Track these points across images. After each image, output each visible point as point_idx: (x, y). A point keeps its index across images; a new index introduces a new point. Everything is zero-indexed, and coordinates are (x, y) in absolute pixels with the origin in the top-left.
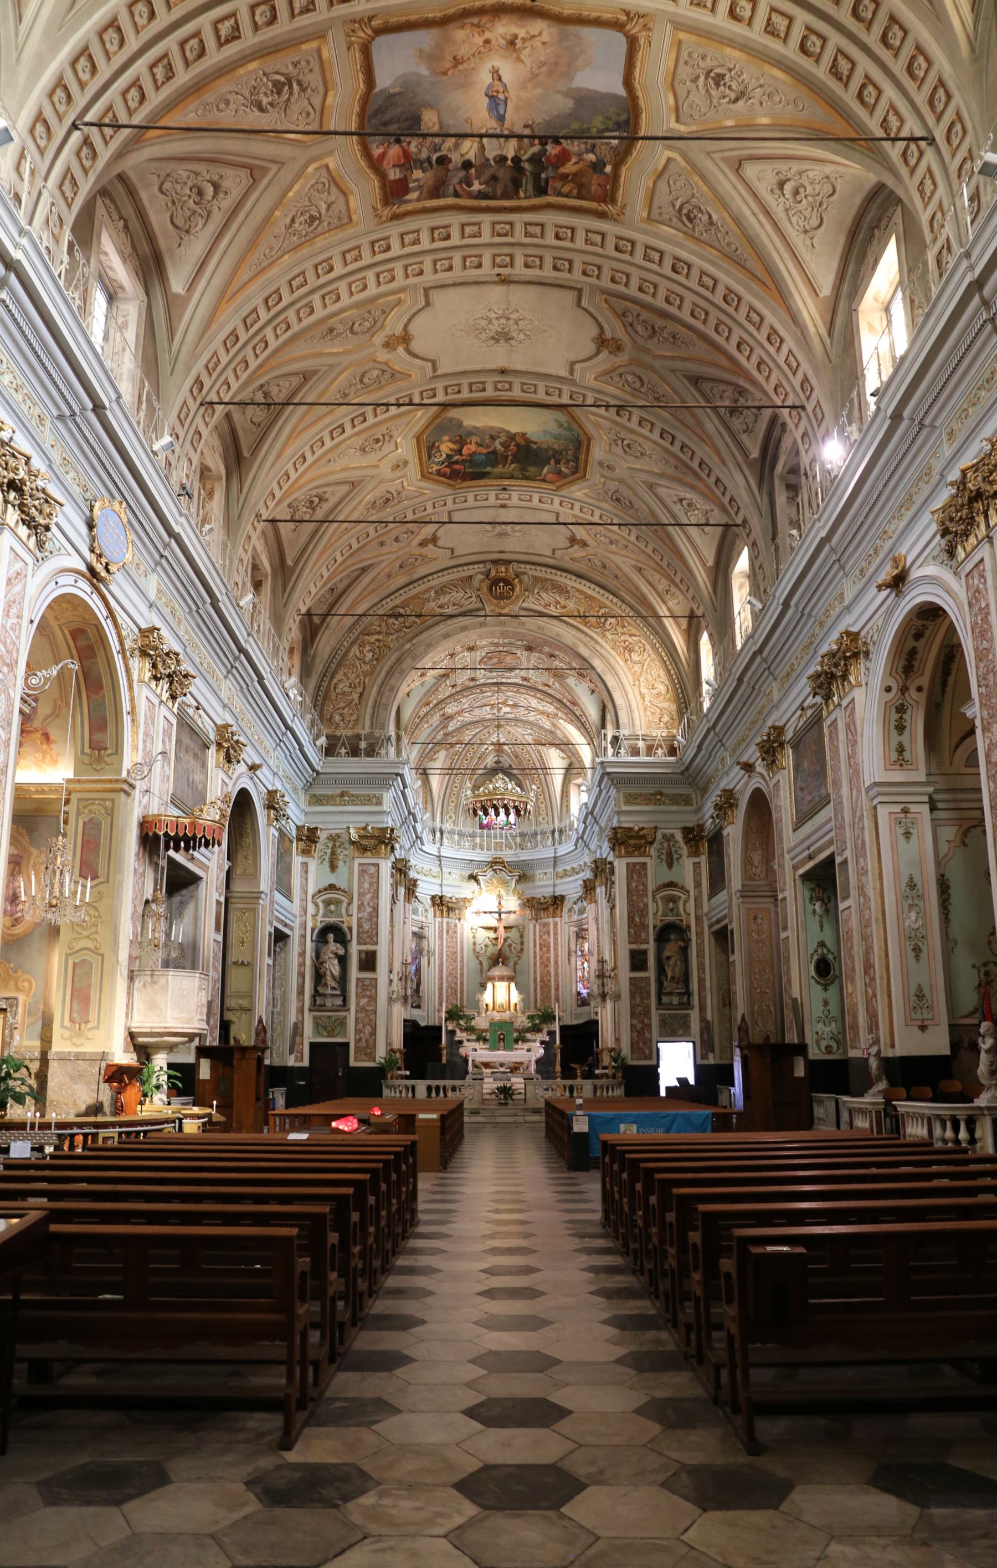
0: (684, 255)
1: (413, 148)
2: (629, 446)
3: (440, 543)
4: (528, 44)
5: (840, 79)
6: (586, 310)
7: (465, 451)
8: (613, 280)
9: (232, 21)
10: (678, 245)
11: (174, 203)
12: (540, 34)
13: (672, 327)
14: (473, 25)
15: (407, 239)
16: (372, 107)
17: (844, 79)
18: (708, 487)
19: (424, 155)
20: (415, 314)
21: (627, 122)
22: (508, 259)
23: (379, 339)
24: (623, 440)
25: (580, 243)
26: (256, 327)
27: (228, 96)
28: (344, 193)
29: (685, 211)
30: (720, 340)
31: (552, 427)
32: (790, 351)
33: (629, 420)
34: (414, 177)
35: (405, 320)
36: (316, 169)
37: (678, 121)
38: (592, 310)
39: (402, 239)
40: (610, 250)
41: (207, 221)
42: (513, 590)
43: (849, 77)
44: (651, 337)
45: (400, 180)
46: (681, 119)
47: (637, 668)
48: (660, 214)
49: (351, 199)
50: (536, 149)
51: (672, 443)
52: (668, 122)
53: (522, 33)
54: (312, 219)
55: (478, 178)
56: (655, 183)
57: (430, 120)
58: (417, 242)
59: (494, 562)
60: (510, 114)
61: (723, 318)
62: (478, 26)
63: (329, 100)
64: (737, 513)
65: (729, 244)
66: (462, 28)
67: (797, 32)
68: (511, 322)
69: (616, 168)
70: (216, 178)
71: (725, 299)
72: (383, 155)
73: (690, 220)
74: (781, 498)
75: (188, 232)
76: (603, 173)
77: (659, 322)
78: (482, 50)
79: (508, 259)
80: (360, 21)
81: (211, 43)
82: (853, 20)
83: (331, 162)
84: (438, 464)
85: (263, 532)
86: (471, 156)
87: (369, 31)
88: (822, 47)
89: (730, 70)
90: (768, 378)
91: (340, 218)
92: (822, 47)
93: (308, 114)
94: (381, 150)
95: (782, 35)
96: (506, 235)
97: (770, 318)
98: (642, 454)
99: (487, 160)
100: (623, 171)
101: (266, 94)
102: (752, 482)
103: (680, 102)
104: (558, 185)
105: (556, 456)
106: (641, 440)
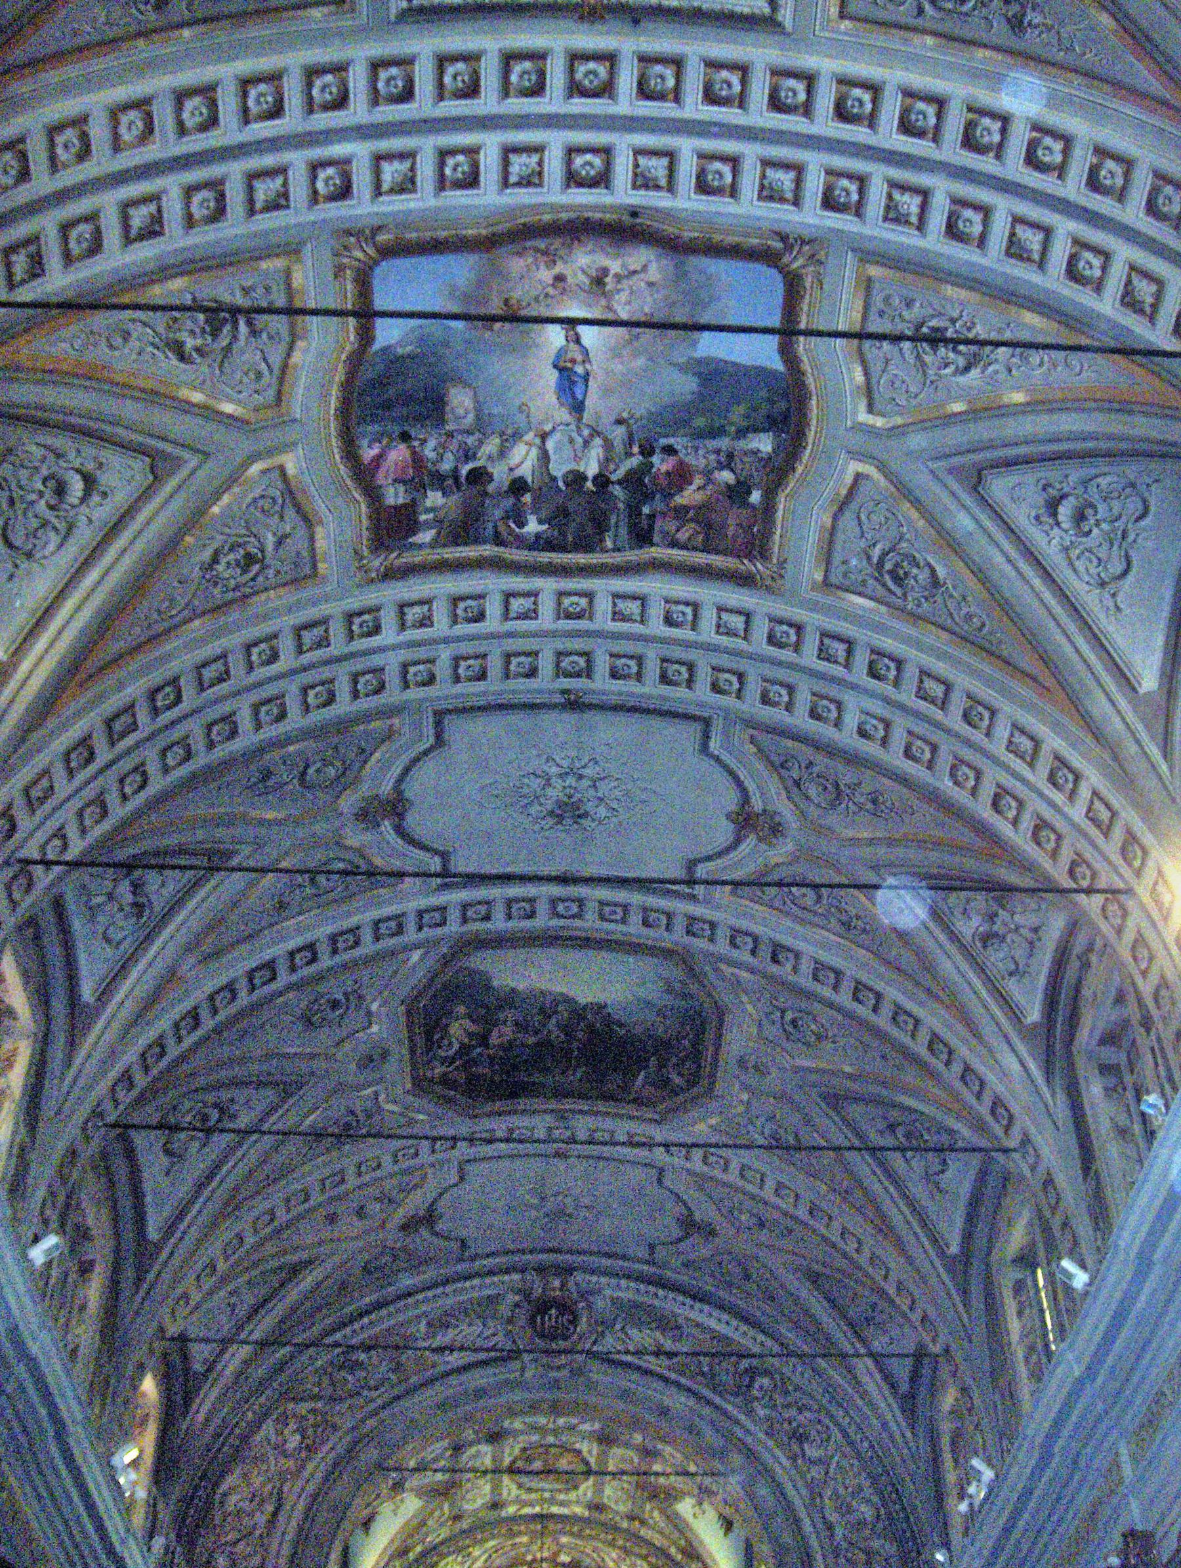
0: (889, 644)
1: (429, 452)
2: (794, 1022)
3: (440, 1226)
4: (625, 284)
5: (1141, 312)
6: (718, 760)
7: (494, 1040)
8: (765, 700)
9: (152, 208)
10: (880, 628)
11: (12, 502)
12: (645, 268)
13: (870, 782)
14: (537, 250)
15: (413, 613)
16: (368, 373)
17: (1148, 310)
18: (950, 1089)
19: (446, 466)
20: (416, 760)
21: (786, 417)
22: (582, 662)
23: (348, 802)
24: (783, 1012)
25: (707, 631)
26: (130, 741)
27: (131, 327)
28: (306, 519)
29: (888, 566)
30: (961, 796)
31: (652, 991)
32: (1095, 793)
33: (795, 970)
34: (429, 503)
35: (397, 770)
36: (263, 472)
37: (871, 409)
38: (726, 757)
39: (402, 614)
40: (759, 642)
41: (66, 537)
42: (574, 1322)
43: (1155, 306)
44: (833, 806)
45: (404, 506)
46: (878, 406)
47: (816, 1472)
48: (845, 575)
49: (320, 532)
50: (635, 461)
51: (875, 1010)
52: (855, 413)
53: (615, 266)
54: (250, 559)
55: (536, 510)
56: (835, 518)
57: (460, 400)
58: (425, 622)
59: (541, 1270)
60: (593, 401)
61: (967, 754)
62: (545, 253)
63: (297, 357)
64: (1007, 1129)
65: (969, 617)
66: (519, 254)
67: (1060, 251)
68: (585, 783)
69: (770, 495)
70: (90, 466)
71: (966, 716)
72: (379, 458)
73: (898, 580)
74: (1094, 1089)
75: (29, 555)
76: (745, 503)
77: (847, 776)
78: (550, 290)
79: (582, 662)
80: (358, 234)
81: (112, 235)
82: (1150, 219)
83: (291, 463)
84: (444, 1061)
85: (165, 1355)
86: (526, 471)
87: (371, 251)
88: (1104, 269)
89: (953, 321)
90: (1054, 854)
91: (296, 565)
92: (1104, 269)
93: (259, 376)
94: (375, 451)
95: (1036, 257)
96: (579, 616)
97: (1053, 742)
98: (819, 1038)
99: (554, 479)
100: (781, 502)
101: (192, 332)
102: (1032, 1066)
103: (874, 381)
104: (671, 526)
105: (663, 1047)
106: (817, 1007)
